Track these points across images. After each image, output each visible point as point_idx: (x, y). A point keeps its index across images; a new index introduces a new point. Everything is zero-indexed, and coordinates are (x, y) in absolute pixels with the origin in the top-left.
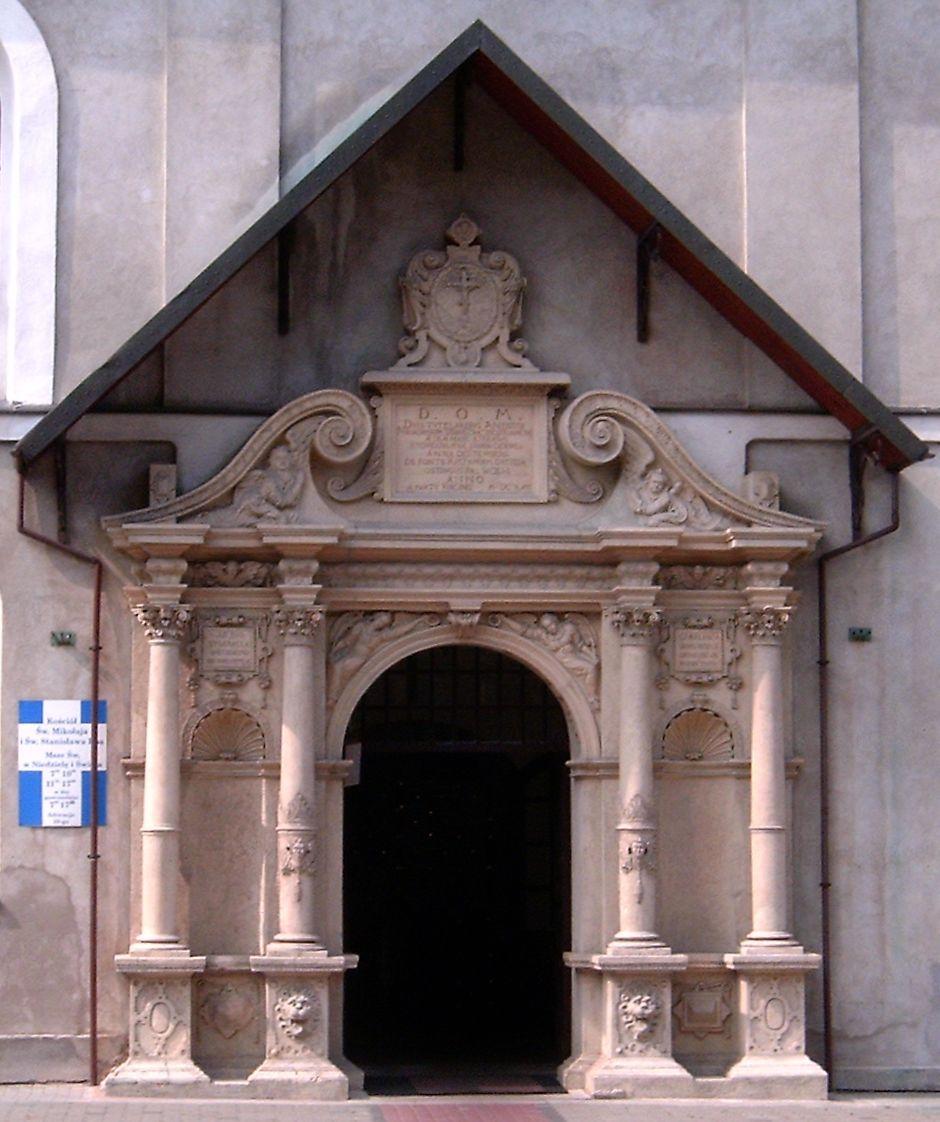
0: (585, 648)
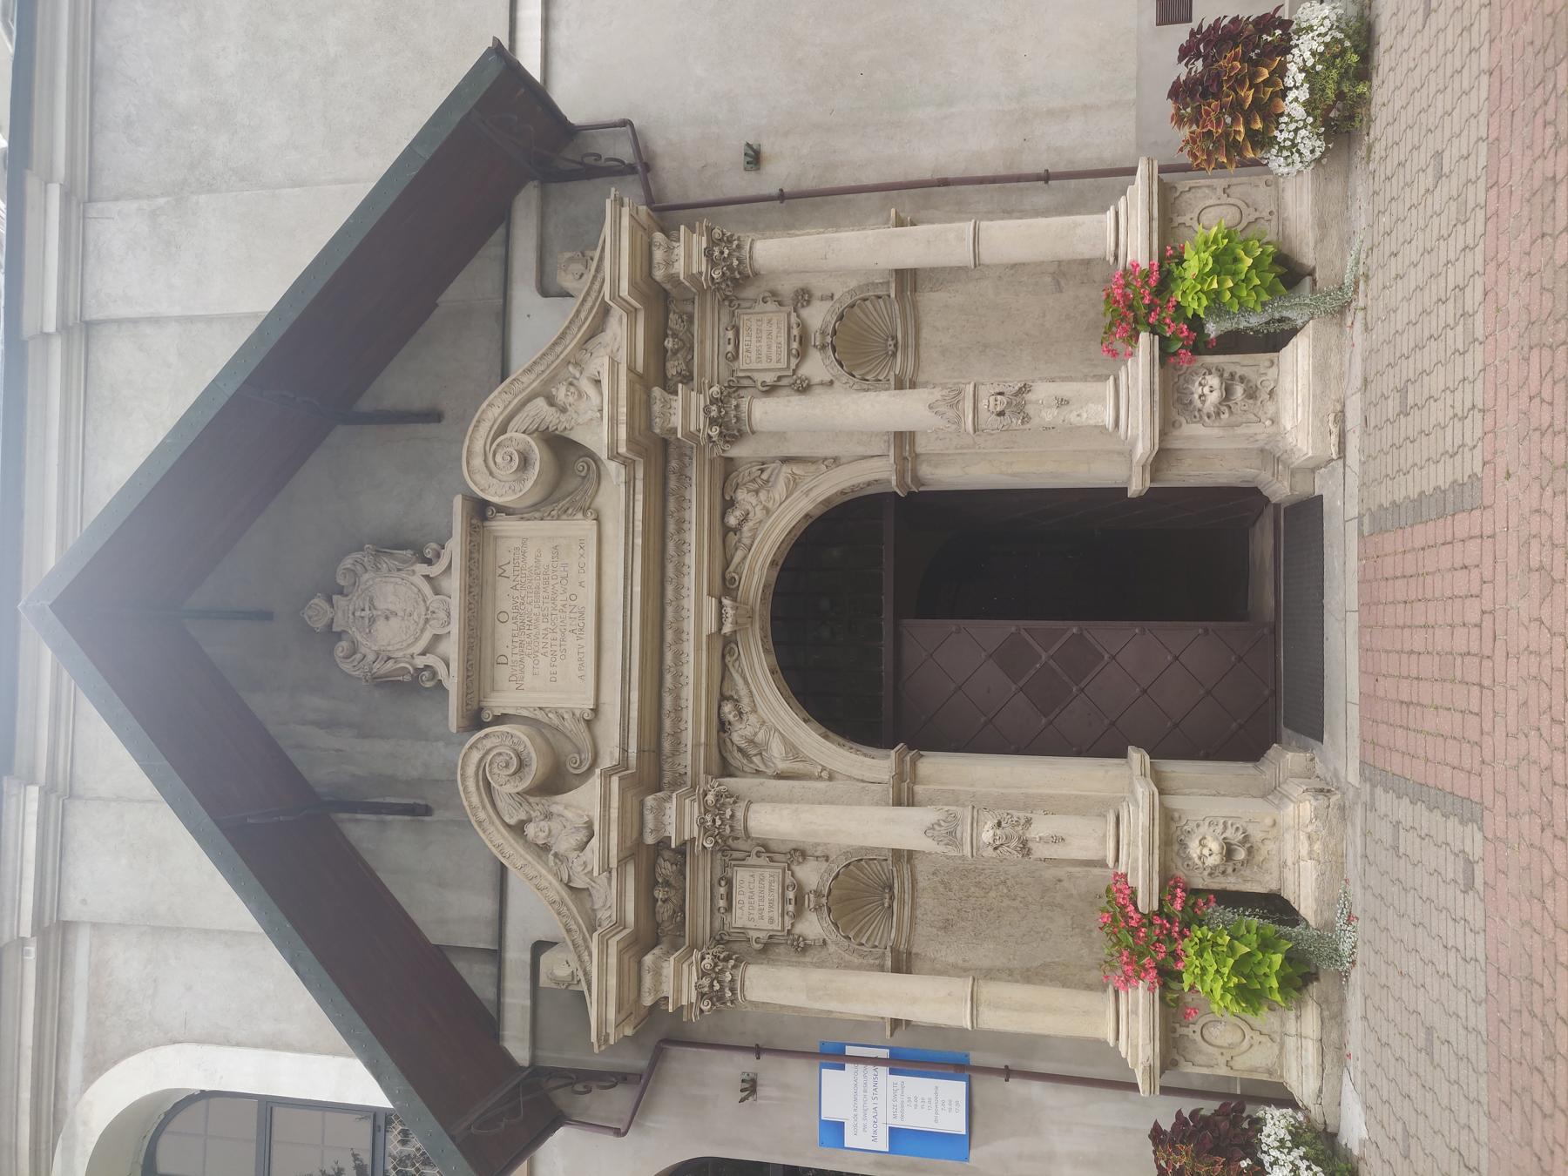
0: (765, 476)
